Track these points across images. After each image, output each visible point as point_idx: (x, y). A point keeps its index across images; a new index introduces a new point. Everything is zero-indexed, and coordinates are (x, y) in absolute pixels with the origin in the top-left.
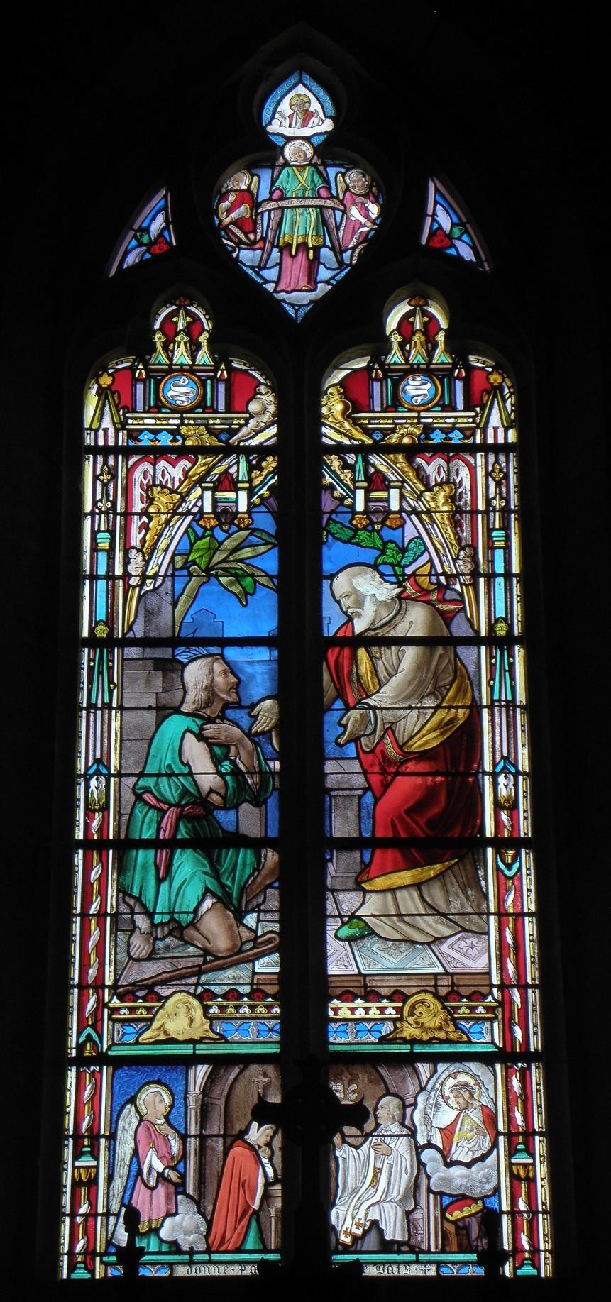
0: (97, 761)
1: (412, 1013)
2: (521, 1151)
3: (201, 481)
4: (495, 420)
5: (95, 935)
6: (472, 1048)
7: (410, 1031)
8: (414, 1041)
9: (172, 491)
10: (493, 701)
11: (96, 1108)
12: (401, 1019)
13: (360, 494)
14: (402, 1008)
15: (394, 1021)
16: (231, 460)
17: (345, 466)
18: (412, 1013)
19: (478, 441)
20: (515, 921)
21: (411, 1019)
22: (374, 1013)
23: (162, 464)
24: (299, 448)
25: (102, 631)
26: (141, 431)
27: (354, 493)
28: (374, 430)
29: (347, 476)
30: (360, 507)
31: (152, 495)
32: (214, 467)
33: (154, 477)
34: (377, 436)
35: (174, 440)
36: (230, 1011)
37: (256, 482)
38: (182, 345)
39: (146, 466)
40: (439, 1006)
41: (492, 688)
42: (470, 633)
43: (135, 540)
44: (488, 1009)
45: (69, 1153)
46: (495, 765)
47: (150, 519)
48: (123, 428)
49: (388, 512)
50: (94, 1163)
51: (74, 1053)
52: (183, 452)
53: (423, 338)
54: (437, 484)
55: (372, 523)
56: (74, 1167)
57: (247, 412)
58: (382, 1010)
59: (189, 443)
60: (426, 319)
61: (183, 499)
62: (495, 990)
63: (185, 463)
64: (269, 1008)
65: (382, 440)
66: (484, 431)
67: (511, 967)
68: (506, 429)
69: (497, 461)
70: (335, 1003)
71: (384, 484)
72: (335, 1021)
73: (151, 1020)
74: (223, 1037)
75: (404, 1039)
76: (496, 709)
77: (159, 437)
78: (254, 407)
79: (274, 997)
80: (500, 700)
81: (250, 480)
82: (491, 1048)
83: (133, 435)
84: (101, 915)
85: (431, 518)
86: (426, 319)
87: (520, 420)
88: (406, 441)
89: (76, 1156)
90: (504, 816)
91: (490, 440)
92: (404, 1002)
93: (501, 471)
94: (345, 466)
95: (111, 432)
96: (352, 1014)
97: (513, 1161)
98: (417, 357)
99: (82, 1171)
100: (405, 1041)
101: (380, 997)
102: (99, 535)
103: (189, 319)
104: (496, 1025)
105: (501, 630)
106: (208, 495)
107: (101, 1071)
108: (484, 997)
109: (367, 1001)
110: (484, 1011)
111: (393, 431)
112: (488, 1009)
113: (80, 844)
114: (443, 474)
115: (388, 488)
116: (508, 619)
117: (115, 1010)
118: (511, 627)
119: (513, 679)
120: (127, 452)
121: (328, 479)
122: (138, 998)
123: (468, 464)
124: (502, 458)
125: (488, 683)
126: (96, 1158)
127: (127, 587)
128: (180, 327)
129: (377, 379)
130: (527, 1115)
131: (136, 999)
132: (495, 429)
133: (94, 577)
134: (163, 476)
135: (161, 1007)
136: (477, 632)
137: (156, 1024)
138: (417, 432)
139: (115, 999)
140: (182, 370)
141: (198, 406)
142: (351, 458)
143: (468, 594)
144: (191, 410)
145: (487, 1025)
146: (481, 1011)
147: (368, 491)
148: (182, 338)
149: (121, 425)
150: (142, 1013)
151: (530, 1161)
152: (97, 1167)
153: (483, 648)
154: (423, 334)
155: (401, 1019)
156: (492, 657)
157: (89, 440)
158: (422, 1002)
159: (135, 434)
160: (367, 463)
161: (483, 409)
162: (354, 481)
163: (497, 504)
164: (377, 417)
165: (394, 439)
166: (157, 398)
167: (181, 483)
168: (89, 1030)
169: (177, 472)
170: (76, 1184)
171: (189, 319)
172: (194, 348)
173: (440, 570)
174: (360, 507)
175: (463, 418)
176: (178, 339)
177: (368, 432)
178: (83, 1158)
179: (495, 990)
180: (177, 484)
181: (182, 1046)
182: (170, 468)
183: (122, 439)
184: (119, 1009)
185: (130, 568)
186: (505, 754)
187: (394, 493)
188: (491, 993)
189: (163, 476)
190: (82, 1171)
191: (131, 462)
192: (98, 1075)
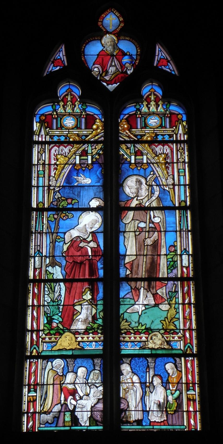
0: (184, 249)
1: (151, 339)
2: (191, 389)
3: (75, 153)
4: (181, 131)
5: (188, 310)
6: (174, 352)
7: (151, 345)
8: (152, 349)
9: (66, 156)
10: (181, 229)
11: (36, 374)
12: (148, 341)
13: (133, 157)
14: (148, 337)
15: (145, 341)
16: (86, 145)
17: (127, 148)
18: (151, 339)
19: (175, 139)
20: (38, 308)
21: (151, 341)
22: (138, 339)
23: (61, 147)
24: (111, 142)
25: (41, 206)
26: (54, 136)
27: (131, 157)
28: (138, 135)
29: (128, 151)
30: (133, 161)
31: (57, 157)
32: (80, 148)
33: (163, 151)
34: (139, 137)
35: (66, 139)
36: (85, 339)
37: (93, 154)
38: (153, 105)
39: (56, 148)
40: (161, 337)
41: (180, 225)
42: (172, 205)
43: (53, 174)
44: (179, 338)
45: (25, 390)
46: (181, 252)
47: (57, 166)
48: (48, 135)
49: (143, 163)
50: (35, 394)
51: (29, 354)
52: (69, 143)
53: (71, 103)
54: (160, 154)
55: (137, 167)
56: (28, 396)
57: (92, 129)
58: (141, 338)
59: (71, 140)
60: (72, 97)
61: (69, 159)
62: (181, 331)
63: (69, 147)
64: (100, 338)
65: (141, 138)
66: (177, 135)
67: (35, 324)
68: (184, 134)
69: (181, 146)
70: (124, 335)
71: (142, 154)
72: (124, 341)
73: (57, 342)
74: (83, 348)
75: (149, 348)
76: (182, 232)
77: (165, 137)
78: (95, 127)
79: (101, 334)
80: (38, 231)
81: (92, 153)
82: (181, 352)
83: (51, 137)
84: (190, 304)
85: (158, 165)
86: (72, 97)
87: (189, 132)
88: (149, 139)
89: (29, 391)
90: (185, 270)
91: (179, 139)
92: (149, 335)
93: (182, 149)
94: (127, 148)
95: (44, 136)
96: (93, 339)
97: (188, 393)
98: (69, 110)
99: (31, 397)
100: (149, 349)
101: (140, 333)
102: (180, 170)
103: (155, 97)
104: (182, 342)
105: (183, 204)
106: (78, 158)
107: (38, 361)
108: (177, 333)
109: (93, 335)
110: (177, 338)
111: (144, 135)
112: (179, 338)
113: (31, 281)
114: (162, 151)
115: (142, 155)
116: (186, 202)
117: (44, 339)
118: (44, 205)
119: (187, 221)
120: (49, 143)
121: (122, 152)
122: (99, 333)
123: (169, 147)
124: (182, 145)
125: (179, 223)
126: (36, 392)
127: (49, 189)
128: (69, 99)
129: (139, 117)
130: (193, 376)
131: (89, 334)
132: (180, 134)
133: (185, 185)
134: (62, 151)
135: (61, 338)
136: (175, 205)
137: (59, 343)
138: (153, 136)
139: (44, 335)
140: (154, 113)
141: (160, 126)
142: (129, 145)
143: (171, 192)
144: (73, 129)
145: (179, 343)
146: (176, 338)
147: (135, 156)
148: (153, 103)
149: (47, 134)
150: (53, 339)
151: (194, 393)
152: (36, 396)
153: (177, 211)
154: (155, 102)
155: (148, 341)
156: (180, 214)
157: (36, 138)
158: (155, 335)
159: (52, 137)
160: (134, 146)
161: (176, 127)
162: (130, 153)
163: (181, 160)
164: (137, 131)
165: (145, 138)
166: (145, 124)
167: (68, 153)
168: (189, 344)
169: (66, 150)
170: (29, 402)
171: (155, 97)
172: (157, 106)
173: (161, 184)
174: (133, 161)
175: (169, 130)
176: (151, 103)
177: (136, 136)
178: (190, 391)
179: (181, 331)
180: (67, 154)
181: (68, 351)
182: (64, 148)
183: (48, 139)
184: (45, 338)
185: (50, 183)
186: (39, 249)
187: (145, 157)
188: (180, 332)
189: (62, 151)
190: (31, 397)
191: (50, 147)
192: (37, 363)
